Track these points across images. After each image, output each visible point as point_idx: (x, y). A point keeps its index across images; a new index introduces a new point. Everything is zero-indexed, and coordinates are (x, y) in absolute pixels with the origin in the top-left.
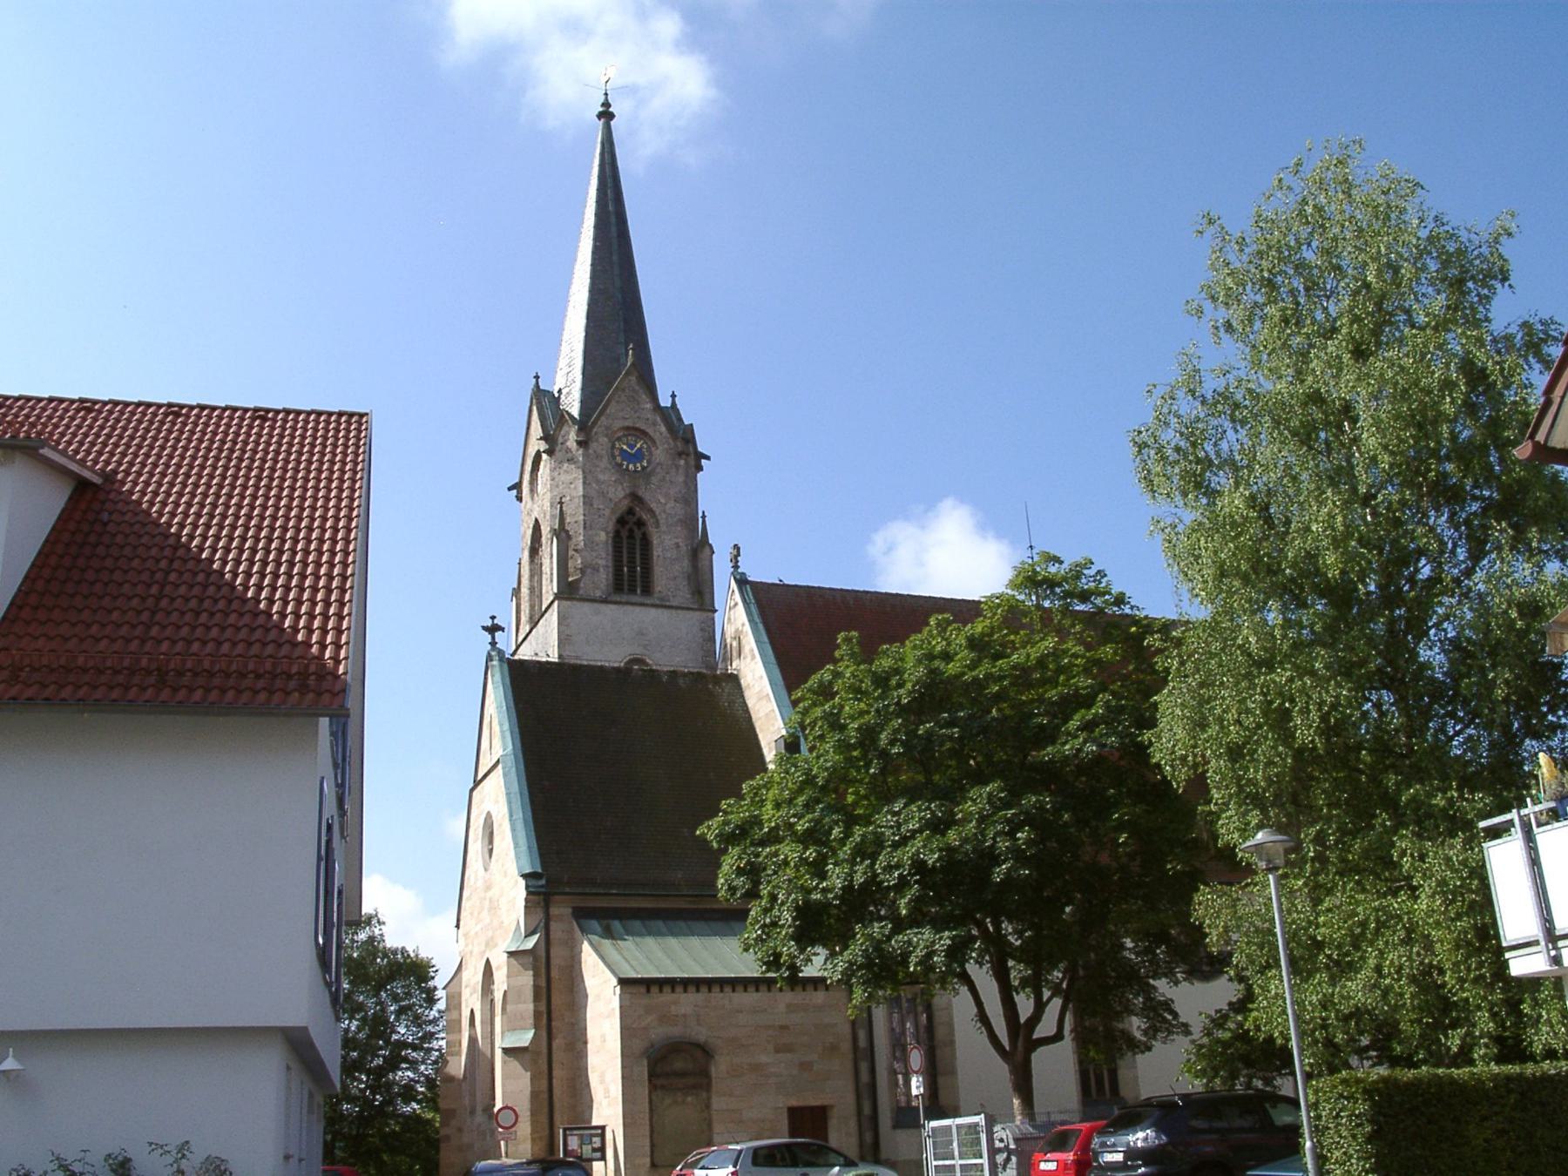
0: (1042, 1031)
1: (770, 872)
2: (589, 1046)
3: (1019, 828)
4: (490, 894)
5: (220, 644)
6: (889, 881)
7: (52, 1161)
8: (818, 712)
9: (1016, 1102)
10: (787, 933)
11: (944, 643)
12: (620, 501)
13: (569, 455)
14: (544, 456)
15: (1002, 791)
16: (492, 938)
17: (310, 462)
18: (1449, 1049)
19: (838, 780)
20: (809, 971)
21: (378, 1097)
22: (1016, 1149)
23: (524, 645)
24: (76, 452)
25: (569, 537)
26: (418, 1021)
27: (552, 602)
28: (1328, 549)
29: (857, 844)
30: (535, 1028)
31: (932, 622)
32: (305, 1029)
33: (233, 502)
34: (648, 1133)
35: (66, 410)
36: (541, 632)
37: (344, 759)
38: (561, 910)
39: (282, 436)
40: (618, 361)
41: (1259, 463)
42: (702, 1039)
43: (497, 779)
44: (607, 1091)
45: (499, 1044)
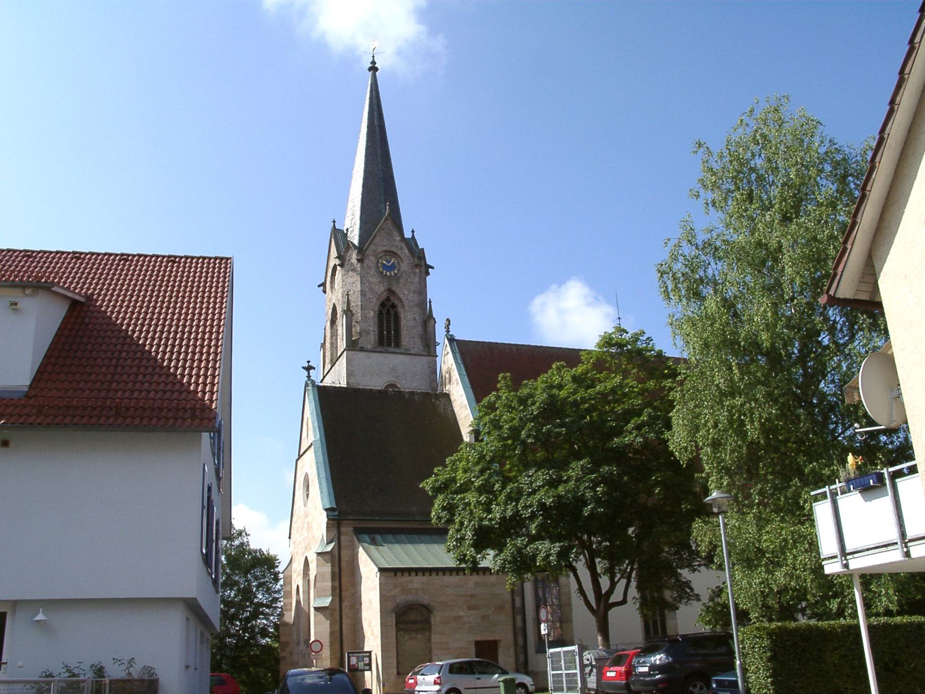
0: (616, 597)
1: (460, 509)
2: (363, 606)
3: (597, 485)
4: (307, 520)
5: (149, 392)
6: (525, 515)
7: (63, 668)
8: (487, 419)
9: (600, 638)
10: (469, 543)
11: (560, 379)
12: (382, 293)
13: (353, 267)
14: (338, 268)
15: (589, 464)
16: (309, 545)
17: (198, 287)
18: (831, 610)
19: (500, 457)
20: (483, 564)
21: (247, 634)
22: (596, 665)
23: (327, 376)
24: (75, 288)
25: (353, 315)
26: (269, 591)
27: (343, 352)
28: (763, 331)
29: (508, 493)
30: (332, 595)
31: (554, 366)
32: (195, 599)
33: (162, 289)
34: (395, 655)
35: (66, 258)
36: (337, 369)
37: (219, 449)
38: (347, 529)
39: (183, 272)
40: (381, 213)
41: (729, 281)
42: (426, 602)
43: (310, 454)
44: (372, 631)
45: (313, 604)
